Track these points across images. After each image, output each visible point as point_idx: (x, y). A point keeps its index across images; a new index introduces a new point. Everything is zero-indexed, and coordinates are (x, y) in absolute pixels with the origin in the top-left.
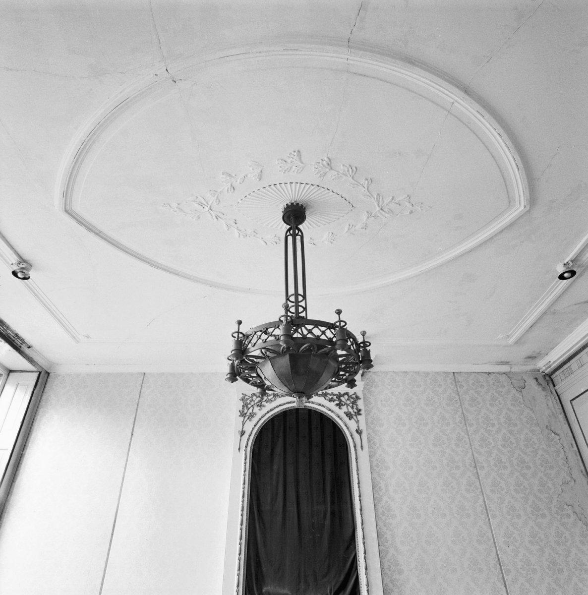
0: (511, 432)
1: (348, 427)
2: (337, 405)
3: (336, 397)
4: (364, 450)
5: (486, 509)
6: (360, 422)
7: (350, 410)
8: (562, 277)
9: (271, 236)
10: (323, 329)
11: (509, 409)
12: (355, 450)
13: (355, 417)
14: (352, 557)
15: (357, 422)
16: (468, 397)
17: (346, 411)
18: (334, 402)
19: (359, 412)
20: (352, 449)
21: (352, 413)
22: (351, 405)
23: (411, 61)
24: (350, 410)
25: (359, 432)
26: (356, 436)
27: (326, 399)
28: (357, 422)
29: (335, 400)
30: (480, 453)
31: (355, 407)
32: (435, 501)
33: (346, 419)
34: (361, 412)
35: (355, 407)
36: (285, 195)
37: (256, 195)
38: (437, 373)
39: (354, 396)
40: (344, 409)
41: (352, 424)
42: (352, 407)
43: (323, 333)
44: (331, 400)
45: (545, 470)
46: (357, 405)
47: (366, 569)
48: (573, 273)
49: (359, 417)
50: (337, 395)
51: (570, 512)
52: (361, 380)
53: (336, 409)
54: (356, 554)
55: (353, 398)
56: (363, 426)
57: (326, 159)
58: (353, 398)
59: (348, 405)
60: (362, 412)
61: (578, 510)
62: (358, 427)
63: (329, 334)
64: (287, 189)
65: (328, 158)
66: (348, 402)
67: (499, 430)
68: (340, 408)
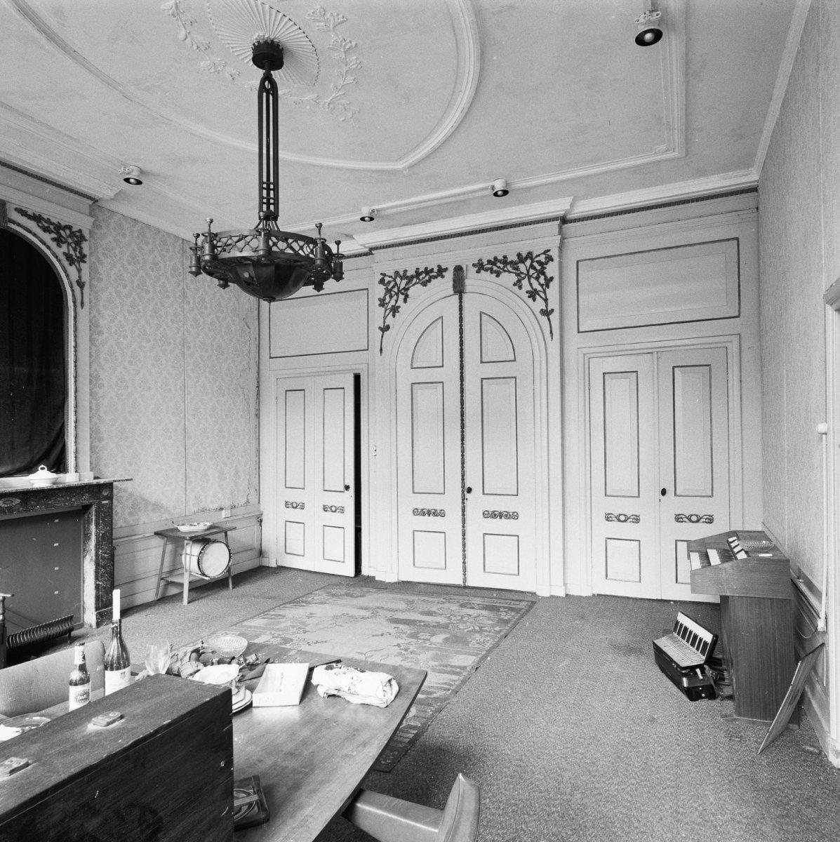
0: (218, 317)
1: (67, 274)
2: (54, 239)
3: (55, 228)
4: (85, 307)
5: (185, 386)
6: (83, 272)
7: (72, 252)
8: (363, 219)
9: (205, 40)
10: (301, 243)
11: (205, 290)
12: (75, 306)
13: (76, 263)
14: (60, 425)
15: (79, 270)
16: (150, 258)
17: (66, 251)
18: (50, 233)
19: (82, 258)
20: (71, 304)
21: (74, 257)
22: (73, 245)
23: (482, 57)
24: (72, 252)
25: (81, 284)
26: (77, 288)
27: (39, 226)
28: (79, 270)
29: (53, 232)
30: (189, 332)
31: (78, 250)
32: (144, 375)
33: (66, 263)
34: (85, 259)
35: (78, 250)
36: (276, 26)
37: (261, 8)
38: (168, 233)
39: (78, 234)
40: (64, 248)
41: (72, 270)
42: (75, 250)
43: (301, 248)
44: (46, 230)
45: (201, 352)
46: (81, 248)
47: (76, 438)
48: (372, 219)
49: (82, 264)
50: (56, 225)
51: (241, 393)
52: (87, 211)
53: (53, 245)
54: (64, 423)
55: (77, 237)
56: (85, 278)
57: (354, 43)
58: (77, 237)
59: (69, 244)
60: (87, 259)
61: (246, 391)
62: (80, 277)
63: (307, 250)
64: (276, 17)
65: (356, 44)
66: (70, 240)
67: (193, 309)
68: (59, 246)
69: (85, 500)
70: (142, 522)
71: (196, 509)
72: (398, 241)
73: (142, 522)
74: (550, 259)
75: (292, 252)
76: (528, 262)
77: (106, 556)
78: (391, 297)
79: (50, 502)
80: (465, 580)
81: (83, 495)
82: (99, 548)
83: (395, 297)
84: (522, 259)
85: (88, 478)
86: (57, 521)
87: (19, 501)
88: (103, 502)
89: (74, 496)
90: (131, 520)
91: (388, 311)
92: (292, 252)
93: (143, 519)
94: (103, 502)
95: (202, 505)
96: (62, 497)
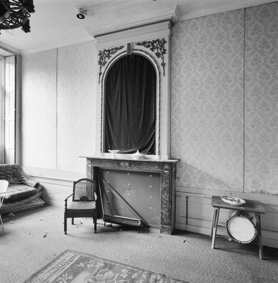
6: (165, 59)
15: (163, 58)
26: (161, 67)
54: (155, 131)
62: (163, 61)
69: (155, 168)
70: (207, 188)
71: (254, 190)
72: (117, 30)
73: (207, 188)
74: (165, 42)
75: (13, 24)
76: (157, 43)
77: (166, 199)
78: (103, 60)
79: (140, 167)
80: (98, 224)
81: (154, 166)
82: (162, 194)
83: (104, 59)
84: (154, 42)
85: (165, 158)
86: (151, 176)
87: (128, 164)
88: (165, 171)
89: (151, 166)
90: (200, 185)
91: (102, 65)
92: (13, 24)
93: (208, 187)
94: (165, 171)
95: (260, 189)
96: (145, 165)
